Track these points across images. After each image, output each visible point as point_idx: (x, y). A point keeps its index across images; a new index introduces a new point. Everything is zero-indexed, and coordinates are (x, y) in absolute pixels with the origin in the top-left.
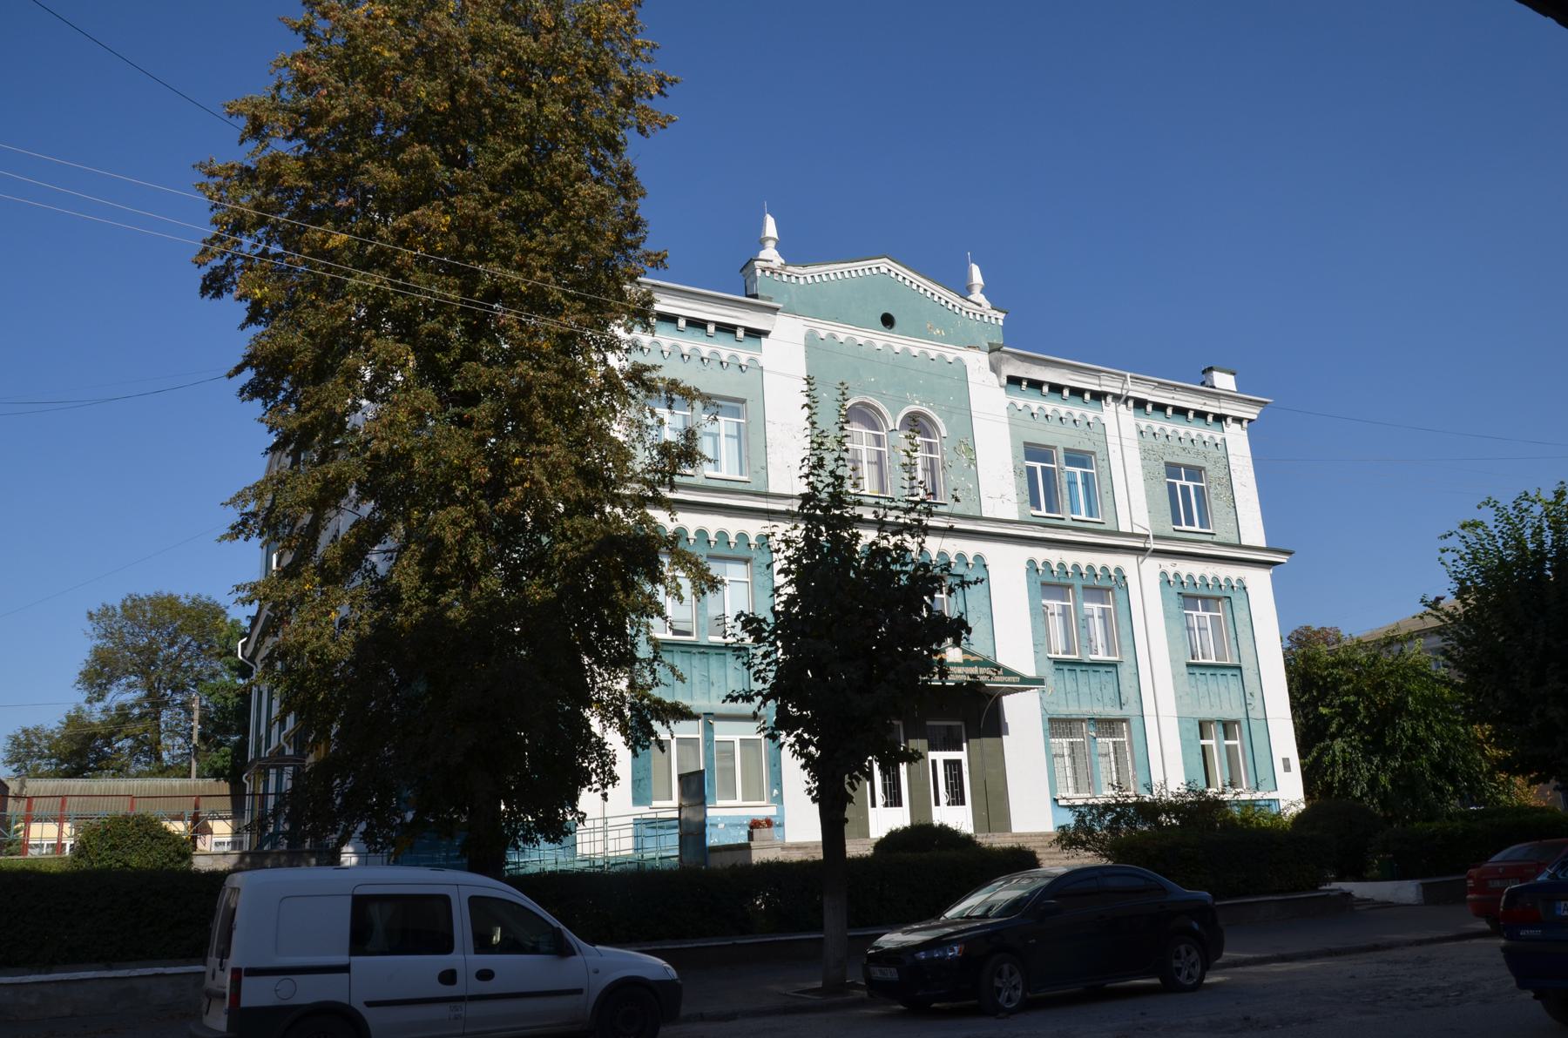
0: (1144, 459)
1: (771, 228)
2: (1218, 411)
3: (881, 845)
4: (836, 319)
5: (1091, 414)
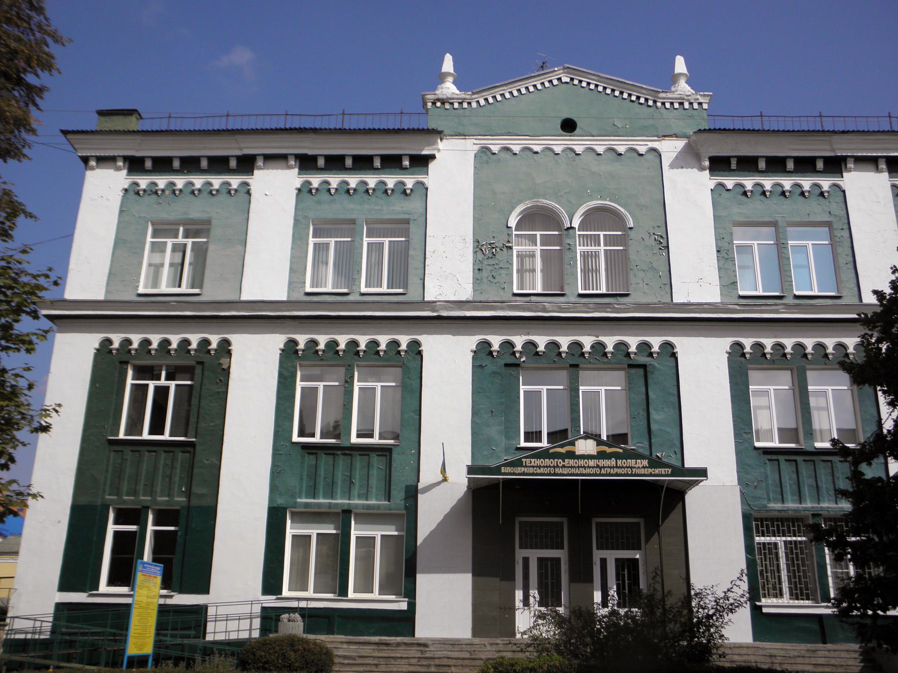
1: (680, 65)
5: (826, 183)
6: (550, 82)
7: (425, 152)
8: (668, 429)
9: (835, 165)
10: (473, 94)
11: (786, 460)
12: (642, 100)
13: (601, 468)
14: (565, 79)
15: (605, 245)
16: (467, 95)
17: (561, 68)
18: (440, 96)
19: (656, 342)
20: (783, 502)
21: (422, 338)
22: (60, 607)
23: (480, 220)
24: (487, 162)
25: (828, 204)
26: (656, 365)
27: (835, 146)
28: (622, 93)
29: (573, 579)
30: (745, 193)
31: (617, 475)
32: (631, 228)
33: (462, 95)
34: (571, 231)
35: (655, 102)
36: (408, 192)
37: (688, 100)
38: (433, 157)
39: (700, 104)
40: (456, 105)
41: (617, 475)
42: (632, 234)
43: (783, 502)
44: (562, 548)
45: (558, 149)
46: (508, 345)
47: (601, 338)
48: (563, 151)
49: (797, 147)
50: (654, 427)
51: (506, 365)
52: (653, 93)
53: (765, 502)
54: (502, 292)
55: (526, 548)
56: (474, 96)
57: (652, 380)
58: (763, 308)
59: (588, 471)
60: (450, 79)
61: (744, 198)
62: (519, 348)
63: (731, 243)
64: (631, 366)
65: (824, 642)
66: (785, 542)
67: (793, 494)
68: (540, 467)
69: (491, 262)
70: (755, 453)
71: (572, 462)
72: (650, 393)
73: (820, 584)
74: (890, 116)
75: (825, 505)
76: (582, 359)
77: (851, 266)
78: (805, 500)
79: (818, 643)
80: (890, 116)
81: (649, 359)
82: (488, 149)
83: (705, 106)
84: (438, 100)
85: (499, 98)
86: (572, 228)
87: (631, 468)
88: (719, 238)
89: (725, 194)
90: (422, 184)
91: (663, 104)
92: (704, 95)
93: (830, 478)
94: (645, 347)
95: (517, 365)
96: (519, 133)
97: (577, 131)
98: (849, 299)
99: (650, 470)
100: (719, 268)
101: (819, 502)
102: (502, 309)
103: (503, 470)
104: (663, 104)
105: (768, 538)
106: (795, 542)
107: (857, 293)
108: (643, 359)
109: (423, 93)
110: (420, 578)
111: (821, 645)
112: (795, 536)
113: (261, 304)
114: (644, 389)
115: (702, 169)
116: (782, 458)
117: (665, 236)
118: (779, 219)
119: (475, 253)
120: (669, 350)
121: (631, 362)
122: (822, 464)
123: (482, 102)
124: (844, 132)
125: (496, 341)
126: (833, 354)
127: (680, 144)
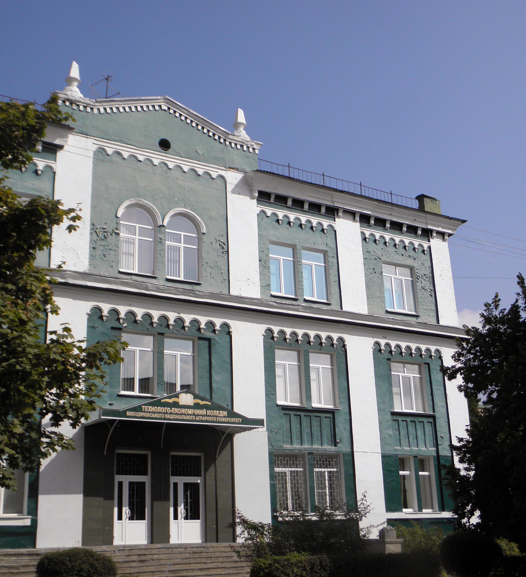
0: (365, 259)
1: (75, 71)
2: (330, 204)
3: (497, 544)
4: (121, 141)
5: (326, 223)
6: (153, 106)
7: (57, 142)
8: (223, 388)
9: (332, 212)
10: (97, 102)
11: (295, 415)
12: (216, 137)
13: (196, 416)
14: (164, 107)
15: (184, 244)
16: (91, 102)
17: (163, 98)
18: (70, 98)
19: (218, 322)
20: (292, 444)
21: (345, 337)
22: (390, 522)
23: (95, 207)
24: (103, 161)
25: (326, 238)
26: (217, 339)
27: (335, 200)
28: (203, 128)
29: (154, 499)
30: (278, 221)
31: (206, 421)
32: (204, 234)
33: (87, 100)
34: (162, 228)
35: (225, 140)
36: (39, 172)
37: (247, 145)
38: (61, 147)
39: (254, 149)
40: (81, 108)
41: (206, 421)
42: (204, 237)
43: (292, 444)
44: (146, 474)
45: (156, 162)
46: (115, 312)
47: (182, 315)
48: (159, 164)
49: (313, 195)
50: (214, 385)
51: (113, 328)
52: (225, 134)
53: (281, 444)
54: (110, 269)
55: (176, 475)
56: (96, 104)
57: (213, 349)
58: (290, 306)
59: (187, 417)
60: (76, 84)
61: (277, 224)
62: (122, 316)
63: (267, 255)
64: (200, 338)
65: (217, 542)
66: (291, 471)
67: (297, 439)
68: (154, 413)
69: (103, 243)
70: (277, 408)
71: (176, 410)
72: (213, 360)
73: (311, 500)
74: (323, 175)
75: (315, 446)
76: (167, 329)
77: (337, 283)
78: (305, 443)
79: (214, 542)
80: (289, 166)
81: (213, 334)
82: (105, 150)
83: (257, 152)
84: (68, 100)
85: (115, 110)
86: (163, 226)
87: (216, 416)
88: (261, 251)
89: (265, 219)
90: (51, 168)
91: (230, 143)
92: (257, 144)
93: (319, 429)
94: (211, 324)
95: (120, 329)
96: (129, 143)
97: (170, 151)
98: (335, 307)
99: (228, 419)
100: (260, 273)
101: (302, 445)
102: (116, 283)
103: (128, 413)
104: (230, 143)
105: (281, 469)
106: (297, 471)
107: (339, 303)
108: (209, 335)
109: (57, 91)
110: (42, 499)
111: (215, 544)
112: (321, 467)
113: (451, 329)
114: (208, 356)
115: (252, 198)
116: (292, 413)
117: (226, 244)
118: (297, 243)
119: (91, 233)
120: (227, 330)
121: (201, 336)
122: (315, 419)
123: (102, 110)
124: (342, 191)
125: (106, 308)
126: (189, 327)
127: (239, 176)
